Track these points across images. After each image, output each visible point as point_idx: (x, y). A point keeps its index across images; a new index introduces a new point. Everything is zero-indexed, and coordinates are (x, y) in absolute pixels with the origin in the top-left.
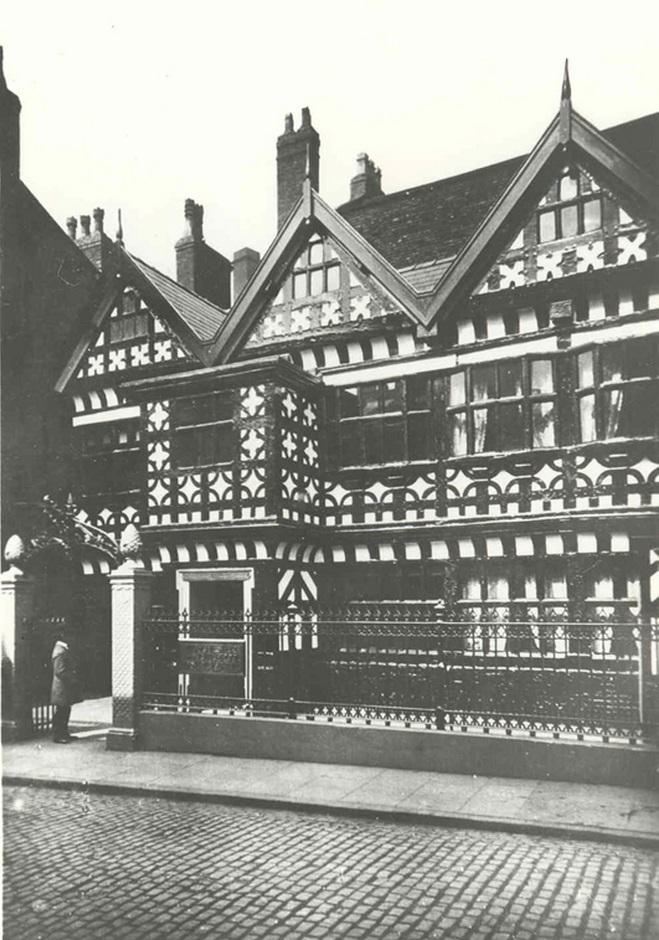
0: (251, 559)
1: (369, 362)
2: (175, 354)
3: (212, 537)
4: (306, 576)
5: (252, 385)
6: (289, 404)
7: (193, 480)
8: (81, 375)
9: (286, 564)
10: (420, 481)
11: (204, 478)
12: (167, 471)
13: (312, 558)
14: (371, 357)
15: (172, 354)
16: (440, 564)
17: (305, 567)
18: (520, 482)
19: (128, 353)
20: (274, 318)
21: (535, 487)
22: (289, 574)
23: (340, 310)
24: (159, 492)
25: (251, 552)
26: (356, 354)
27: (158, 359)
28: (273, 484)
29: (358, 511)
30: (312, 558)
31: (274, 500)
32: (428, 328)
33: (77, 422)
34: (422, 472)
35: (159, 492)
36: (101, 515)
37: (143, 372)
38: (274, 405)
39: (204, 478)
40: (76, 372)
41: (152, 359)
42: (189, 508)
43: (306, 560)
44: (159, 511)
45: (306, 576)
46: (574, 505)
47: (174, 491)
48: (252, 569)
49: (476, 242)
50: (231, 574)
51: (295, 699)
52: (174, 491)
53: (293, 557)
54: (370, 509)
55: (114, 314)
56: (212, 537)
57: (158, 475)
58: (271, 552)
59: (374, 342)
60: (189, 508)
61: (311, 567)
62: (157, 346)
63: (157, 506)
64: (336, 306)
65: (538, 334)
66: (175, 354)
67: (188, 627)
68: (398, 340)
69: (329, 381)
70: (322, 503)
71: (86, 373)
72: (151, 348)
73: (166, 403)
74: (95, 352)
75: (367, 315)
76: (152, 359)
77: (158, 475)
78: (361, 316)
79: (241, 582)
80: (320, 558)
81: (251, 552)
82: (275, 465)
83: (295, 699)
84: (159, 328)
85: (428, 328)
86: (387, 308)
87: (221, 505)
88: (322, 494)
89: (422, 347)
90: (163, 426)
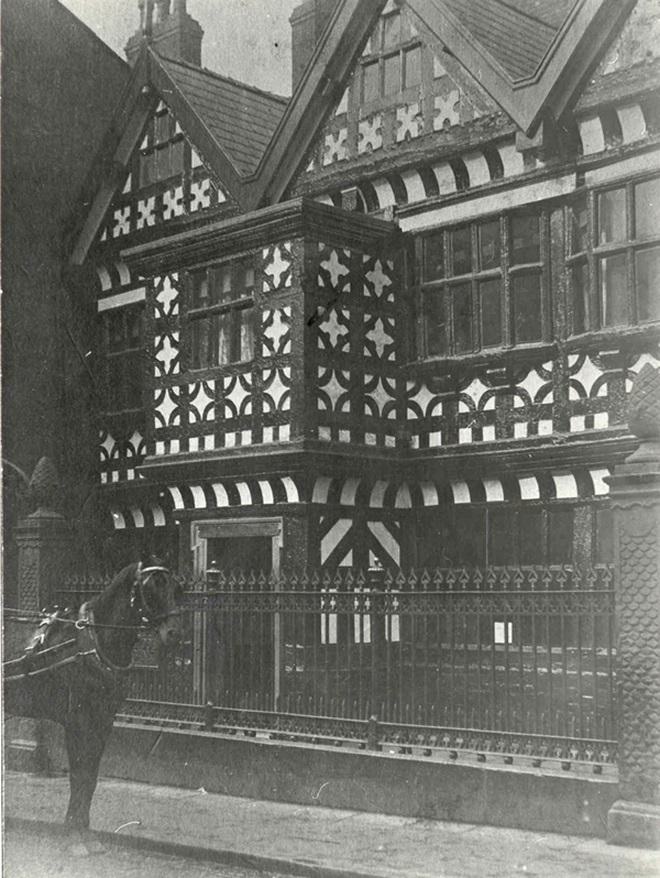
0: (189, 509)
1: (466, 191)
2: (214, 198)
3: (231, 470)
4: (377, 528)
5: (275, 243)
6: (335, 268)
7: (243, 380)
8: (104, 238)
9: (336, 511)
10: (533, 375)
11: (219, 383)
12: (177, 376)
13: (390, 498)
14: (467, 184)
15: (211, 200)
16: (568, 506)
17: (376, 516)
18: (500, 395)
19: (159, 200)
20: (336, 136)
21: (463, 408)
22: (343, 526)
23: (420, 114)
24: (167, 407)
25: (279, 492)
26: (479, 172)
27: (194, 207)
28: (307, 390)
29: (450, 425)
30: (390, 498)
31: (306, 411)
32: (531, 134)
33: (104, 305)
34: (533, 361)
35: (167, 407)
36: (468, 391)
37: (149, 233)
38: (309, 274)
39: (219, 383)
40: (99, 235)
41: (187, 207)
42: (201, 429)
43: (376, 503)
44: (166, 435)
45: (377, 528)
46: (567, 427)
47: (184, 404)
48: (281, 518)
49: (300, 100)
50: (250, 525)
51: (379, 719)
52: (184, 404)
53: (348, 499)
54: (579, 409)
55: (145, 145)
56: (231, 470)
57: (168, 381)
58: (305, 491)
59: (407, 177)
60: (201, 429)
61: (387, 515)
62: (194, 189)
63: (164, 429)
64: (415, 109)
65: (456, 196)
66: (214, 198)
67: (367, 603)
68: (406, 181)
69: (407, 225)
70: (402, 415)
71: (110, 234)
72: (187, 190)
73: (175, 276)
74: (120, 202)
75: (455, 120)
76: (187, 207)
77: (168, 381)
78: (447, 121)
79: (269, 539)
80: (403, 501)
81: (279, 492)
82: (313, 355)
83: (379, 719)
84: (196, 161)
85: (531, 134)
86: (483, 107)
87: (239, 423)
88: (403, 401)
89: (535, 164)
90: (171, 310)
